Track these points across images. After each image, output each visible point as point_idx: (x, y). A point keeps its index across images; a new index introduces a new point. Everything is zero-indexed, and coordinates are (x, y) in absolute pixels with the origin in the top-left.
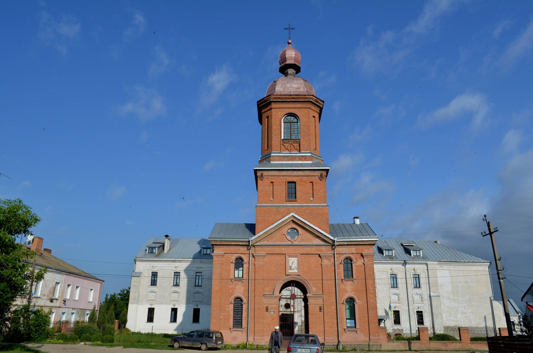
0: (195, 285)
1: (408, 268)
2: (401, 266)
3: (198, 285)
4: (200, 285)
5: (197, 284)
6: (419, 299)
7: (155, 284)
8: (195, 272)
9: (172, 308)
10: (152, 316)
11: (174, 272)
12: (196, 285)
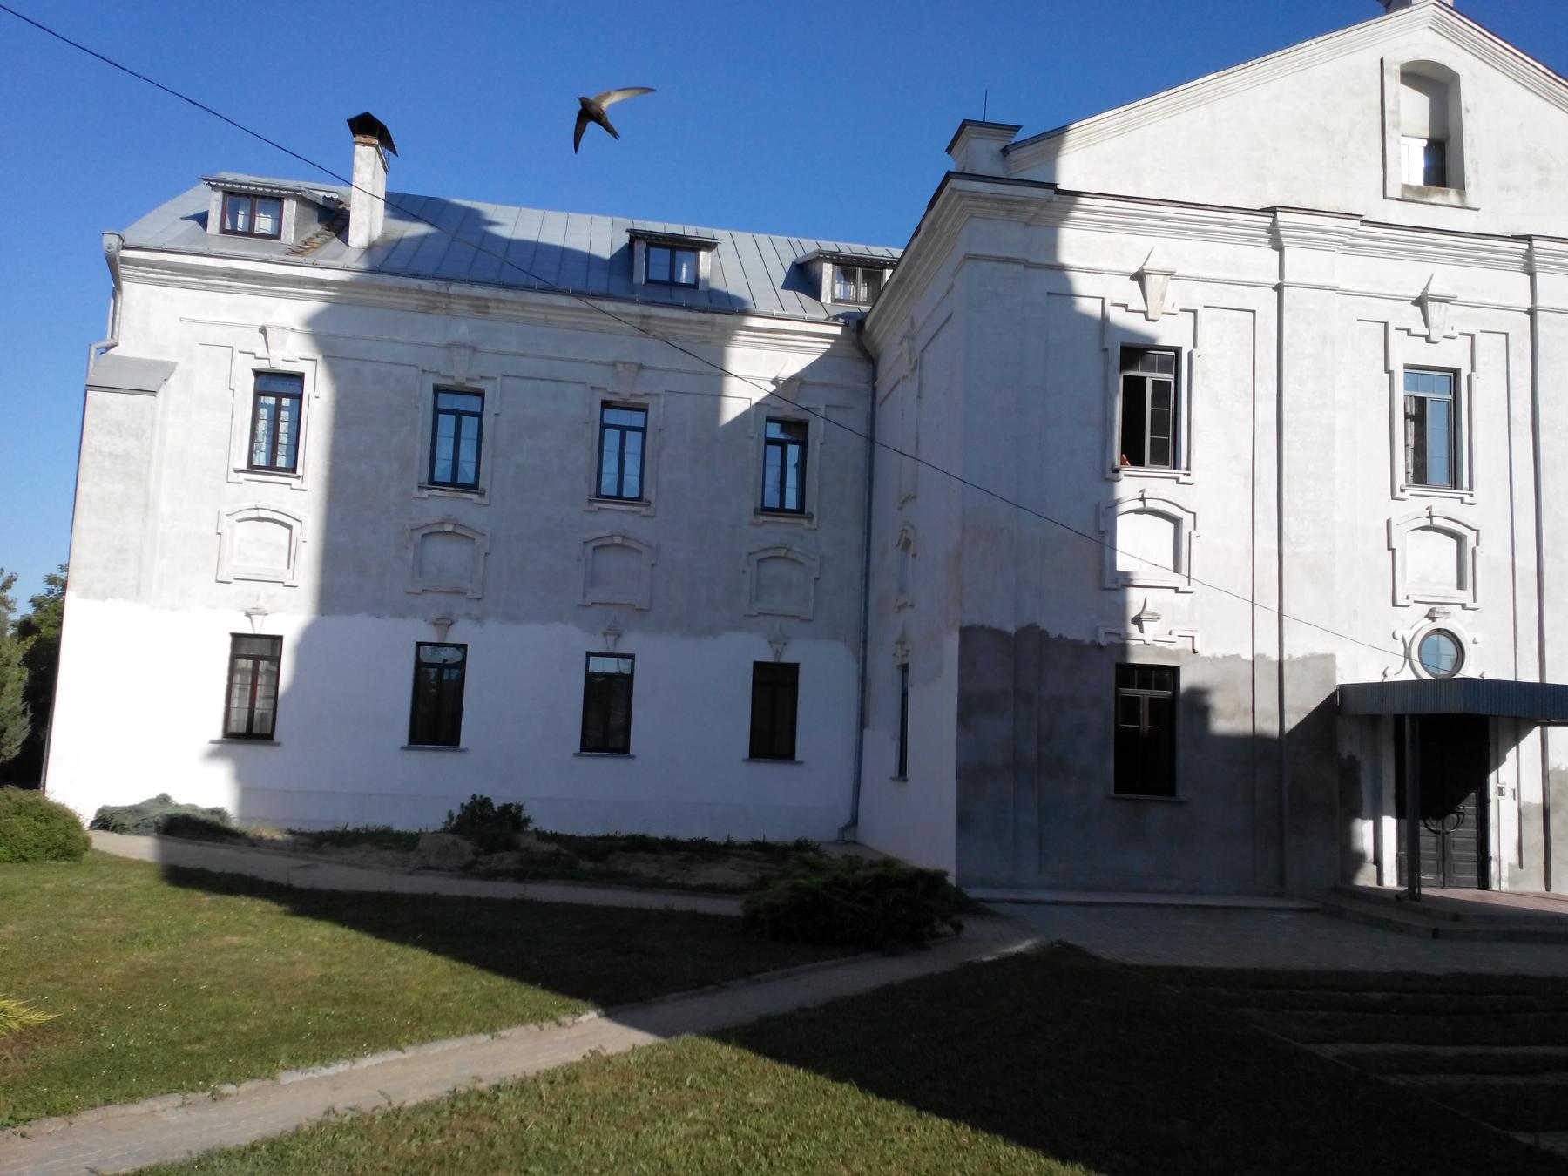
0: (425, 478)
3: (614, 493)
4: (471, 481)
5: (609, 486)
8: (431, 381)
12: (438, 477)
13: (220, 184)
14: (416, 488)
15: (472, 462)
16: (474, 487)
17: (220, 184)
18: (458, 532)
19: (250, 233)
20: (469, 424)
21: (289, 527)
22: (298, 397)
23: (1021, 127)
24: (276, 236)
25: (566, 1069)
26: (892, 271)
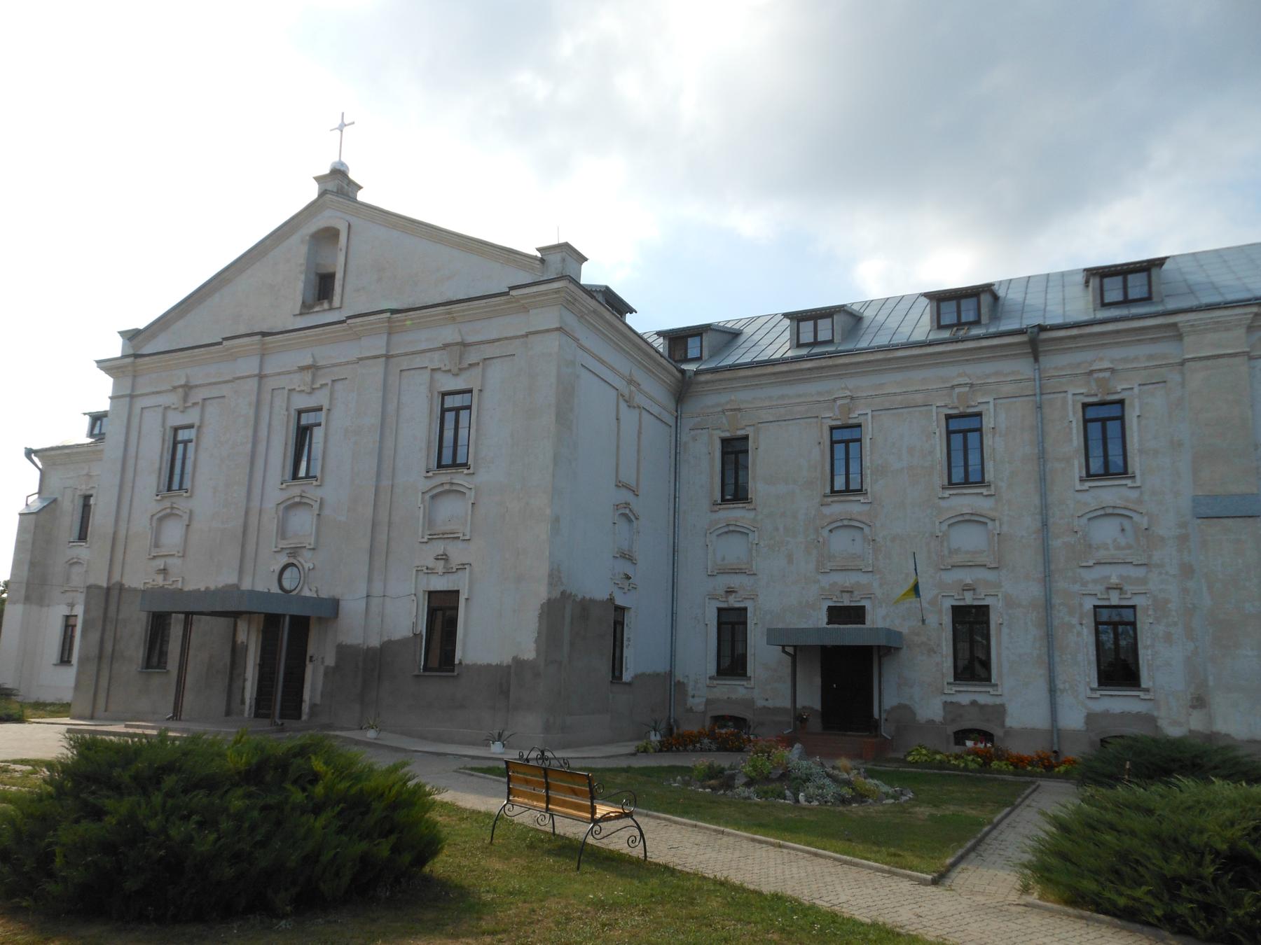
0: (828, 490)
9: (952, 606)
14: (1077, 481)
15: (1100, 457)
16: (981, 482)
18: (973, 519)
20: (1113, 427)
22: (1121, 418)
23: (119, 332)
25: (725, 901)
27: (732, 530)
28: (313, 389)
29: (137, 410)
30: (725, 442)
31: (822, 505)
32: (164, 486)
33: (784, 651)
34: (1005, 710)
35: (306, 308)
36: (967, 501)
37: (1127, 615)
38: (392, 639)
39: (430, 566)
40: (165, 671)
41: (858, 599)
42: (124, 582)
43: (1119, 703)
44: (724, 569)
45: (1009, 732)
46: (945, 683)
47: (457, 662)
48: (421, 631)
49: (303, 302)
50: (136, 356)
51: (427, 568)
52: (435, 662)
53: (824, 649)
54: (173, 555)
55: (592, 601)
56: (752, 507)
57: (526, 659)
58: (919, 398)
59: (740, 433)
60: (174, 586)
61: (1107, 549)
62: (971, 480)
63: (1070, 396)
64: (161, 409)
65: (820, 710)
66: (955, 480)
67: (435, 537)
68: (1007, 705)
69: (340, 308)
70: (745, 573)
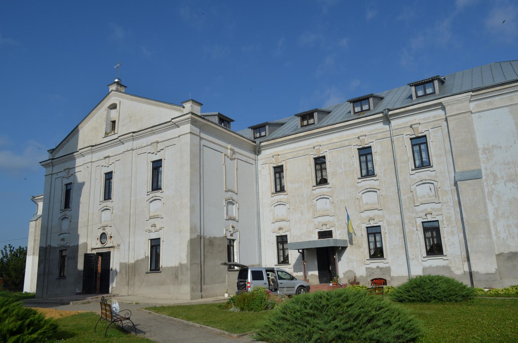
1: (398, 125)
2: (380, 126)
6: (428, 194)
7: (282, 190)
9: (318, 232)
10: (42, 266)
11: (411, 139)
13: (414, 84)
17: (414, 84)
19: (426, 95)
20: (423, 147)
21: (433, 184)
22: (426, 143)
24: (434, 93)
26: (306, 121)
27: (280, 204)
28: (69, 176)
29: (53, 179)
30: (315, 159)
31: (312, 190)
32: (63, 207)
33: (299, 252)
34: (390, 269)
35: (107, 134)
36: (369, 183)
37: (435, 224)
38: (139, 259)
39: (150, 230)
40: (64, 278)
41: (329, 227)
42: (51, 245)
43: (435, 262)
44: (277, 220)
45: (392, 278)
46: (366, 260)
47: (160, 267)
48: (148, 256)
49: (106, 133)
50: (53, 159)
51: (149, 230)
52: (153, 268)
53: (318, 249)
54: (66, 233)
55: (215, 238)
56: (286, 193)
57: (183, 263)
58: (346, 143)
59: (280, 164)
60: (67, 245)
61: (426, 198)
62: (424, 165)
63: (404, 136)
64: (61, 178)
65: (318, 275)
66: (363, 175)
67: (151, 218)
68: (391, 267)
69: (117, 133)
70: (285, 221)
